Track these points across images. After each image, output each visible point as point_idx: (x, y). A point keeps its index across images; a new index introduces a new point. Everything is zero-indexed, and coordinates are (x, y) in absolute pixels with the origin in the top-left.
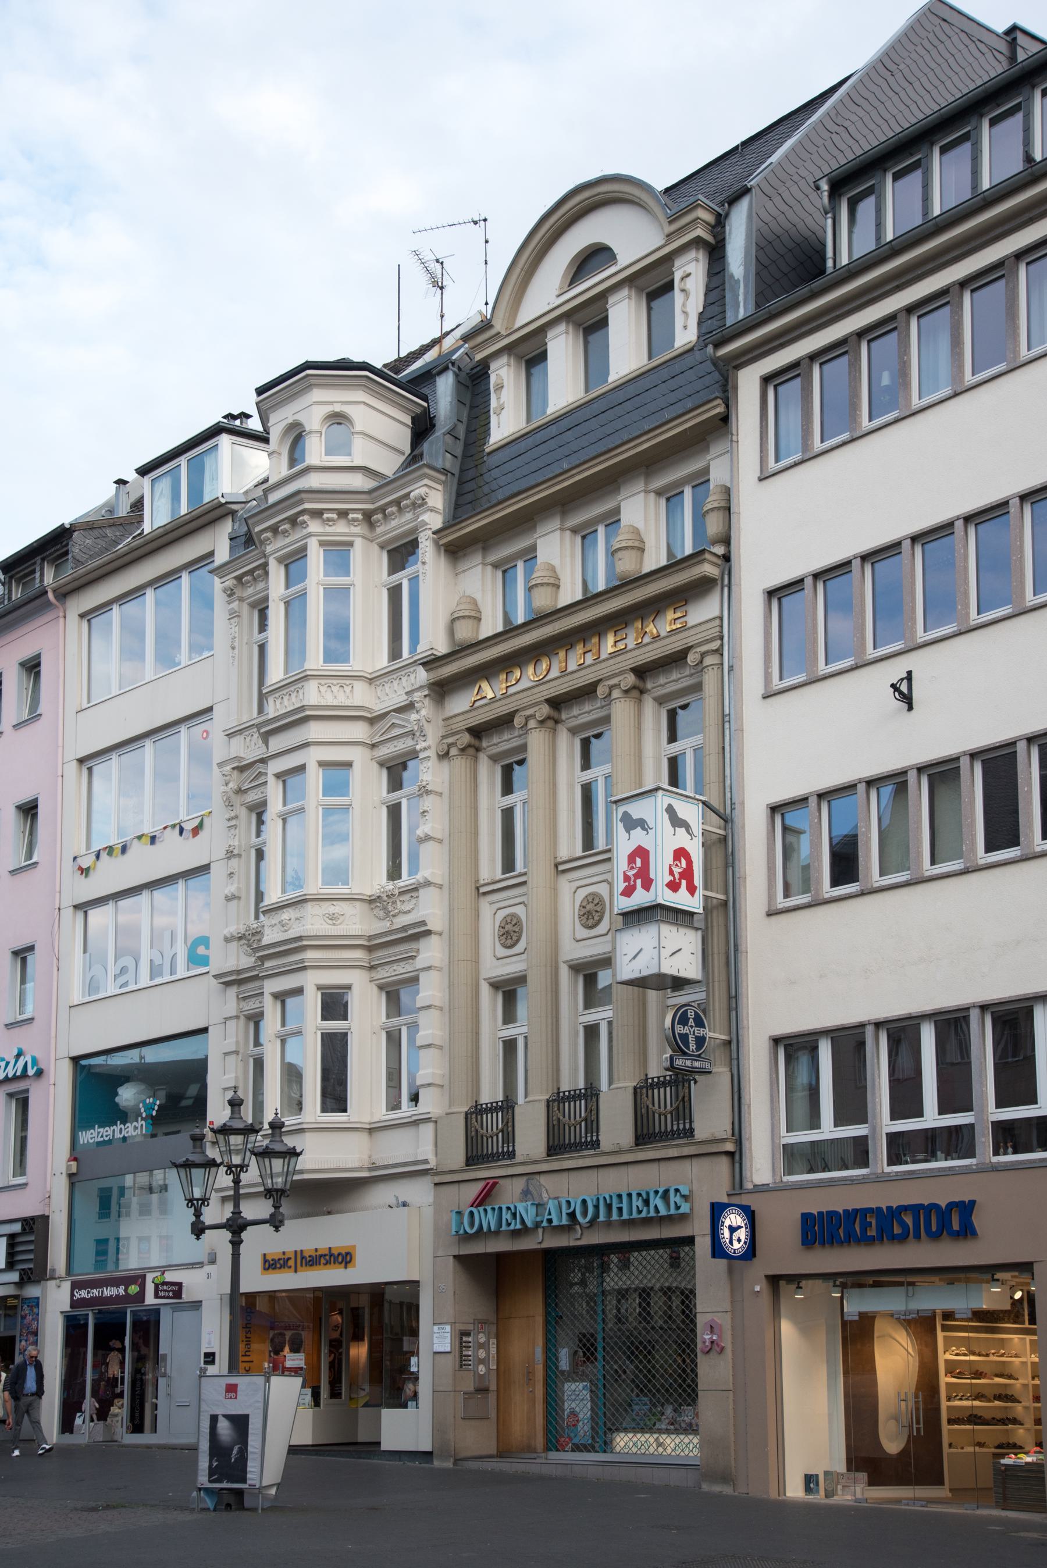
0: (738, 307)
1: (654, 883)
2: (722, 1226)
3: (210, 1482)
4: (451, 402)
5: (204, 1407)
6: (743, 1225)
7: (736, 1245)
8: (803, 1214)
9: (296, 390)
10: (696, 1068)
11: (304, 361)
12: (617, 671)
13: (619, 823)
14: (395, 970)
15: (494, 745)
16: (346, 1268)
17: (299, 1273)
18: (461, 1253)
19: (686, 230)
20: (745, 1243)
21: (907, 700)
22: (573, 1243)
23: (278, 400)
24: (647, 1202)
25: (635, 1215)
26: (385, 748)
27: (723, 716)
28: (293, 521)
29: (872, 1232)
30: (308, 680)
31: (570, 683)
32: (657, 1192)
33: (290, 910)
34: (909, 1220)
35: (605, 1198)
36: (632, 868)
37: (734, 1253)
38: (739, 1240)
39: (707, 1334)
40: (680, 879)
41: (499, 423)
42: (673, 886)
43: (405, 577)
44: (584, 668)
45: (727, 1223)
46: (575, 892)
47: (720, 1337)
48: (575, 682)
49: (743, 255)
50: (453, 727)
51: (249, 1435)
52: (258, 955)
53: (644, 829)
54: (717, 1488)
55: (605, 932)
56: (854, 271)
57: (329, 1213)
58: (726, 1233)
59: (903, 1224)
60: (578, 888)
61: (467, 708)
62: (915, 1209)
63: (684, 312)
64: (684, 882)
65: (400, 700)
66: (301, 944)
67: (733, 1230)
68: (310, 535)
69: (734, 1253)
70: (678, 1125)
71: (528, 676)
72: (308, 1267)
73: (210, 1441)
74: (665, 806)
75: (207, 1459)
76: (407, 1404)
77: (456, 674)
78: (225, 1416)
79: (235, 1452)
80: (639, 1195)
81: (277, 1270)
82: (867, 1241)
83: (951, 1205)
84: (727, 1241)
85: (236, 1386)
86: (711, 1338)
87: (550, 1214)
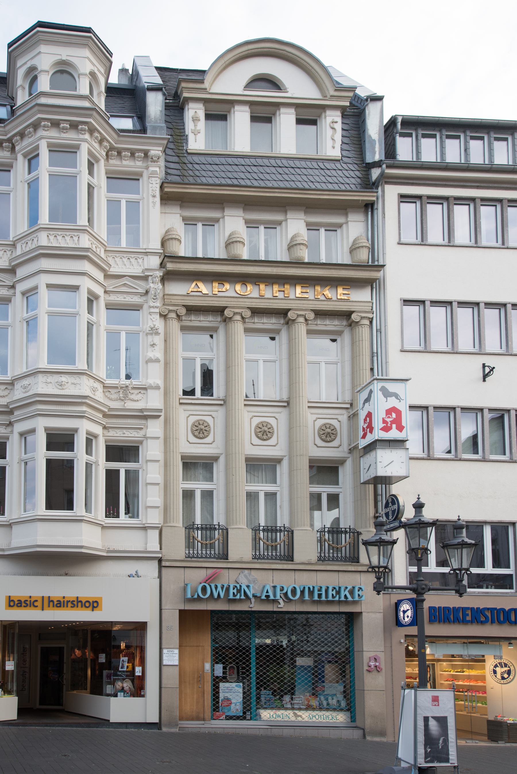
0: (375, 153)
3: (426, 762)
4: (161, 111)
5: (419, 711)
6: (410, 608)
7: (407, 619)
8: (429, 607)
9: (73, 41)
10: (392, 527)
11: (88, 26)
12: (304, 308)
13: (379, 392)
14: (124, 434)
15: (199, 321)
16: (93, 610)
17: (44, 611)
18: (186, 608)
19: (196, 91)
20: (411, 617)
21: (485, 377)
22: (276, 609)
23: (56, 39)
24: (338, 592)
25: (330, 598)
26: (115, 297)
27: (373, 353)
28: (74, 126)
29: (469, 618)
30: (84, 233)
31: (268, 304)
32: (346, 588)
33: (67, 376)
34: (489, 614)
35: (309, 588)
36: (389, 417)
37: (406, 623)
38: (408, 617)
39: (372, 662)
40: (391, 424)
41: (196, 140)
43: (125, 199)
44: (262, 298)
45: (402, 609)
46: (188, 417)
47: (380, 664)
48: (271, 304)
49: (378, 129)
50: (172, 301)
51: (449, 730)
53: (397, 398)
54: (377, 739)
55: (337, 446)
56: (448, 167)
57: (66, 574)
58: (401, 614)
59: (486, 617)
60: (274, 417)
61: (185, 293)
62: (492, 610)
63: (333, 139)
64: (394, 426)
65: (137, 271)
66: (84, 401)
67: (404, 612)
68: (41, 138)
69: (406, 623)
70: (337, 554)
71: (251, 290)
72: (55, 608)
73: (425, 735)
75: (423, 747)
76: (117, 694)
77: (192, 271)
78: (433, 717)
79: (441, 742)
81: (23, 608)
82: (464, 622)
83: (511, 610)
84: (402, 618)
85: (438, 697)
86: (375, 664)
87: (267, 592)
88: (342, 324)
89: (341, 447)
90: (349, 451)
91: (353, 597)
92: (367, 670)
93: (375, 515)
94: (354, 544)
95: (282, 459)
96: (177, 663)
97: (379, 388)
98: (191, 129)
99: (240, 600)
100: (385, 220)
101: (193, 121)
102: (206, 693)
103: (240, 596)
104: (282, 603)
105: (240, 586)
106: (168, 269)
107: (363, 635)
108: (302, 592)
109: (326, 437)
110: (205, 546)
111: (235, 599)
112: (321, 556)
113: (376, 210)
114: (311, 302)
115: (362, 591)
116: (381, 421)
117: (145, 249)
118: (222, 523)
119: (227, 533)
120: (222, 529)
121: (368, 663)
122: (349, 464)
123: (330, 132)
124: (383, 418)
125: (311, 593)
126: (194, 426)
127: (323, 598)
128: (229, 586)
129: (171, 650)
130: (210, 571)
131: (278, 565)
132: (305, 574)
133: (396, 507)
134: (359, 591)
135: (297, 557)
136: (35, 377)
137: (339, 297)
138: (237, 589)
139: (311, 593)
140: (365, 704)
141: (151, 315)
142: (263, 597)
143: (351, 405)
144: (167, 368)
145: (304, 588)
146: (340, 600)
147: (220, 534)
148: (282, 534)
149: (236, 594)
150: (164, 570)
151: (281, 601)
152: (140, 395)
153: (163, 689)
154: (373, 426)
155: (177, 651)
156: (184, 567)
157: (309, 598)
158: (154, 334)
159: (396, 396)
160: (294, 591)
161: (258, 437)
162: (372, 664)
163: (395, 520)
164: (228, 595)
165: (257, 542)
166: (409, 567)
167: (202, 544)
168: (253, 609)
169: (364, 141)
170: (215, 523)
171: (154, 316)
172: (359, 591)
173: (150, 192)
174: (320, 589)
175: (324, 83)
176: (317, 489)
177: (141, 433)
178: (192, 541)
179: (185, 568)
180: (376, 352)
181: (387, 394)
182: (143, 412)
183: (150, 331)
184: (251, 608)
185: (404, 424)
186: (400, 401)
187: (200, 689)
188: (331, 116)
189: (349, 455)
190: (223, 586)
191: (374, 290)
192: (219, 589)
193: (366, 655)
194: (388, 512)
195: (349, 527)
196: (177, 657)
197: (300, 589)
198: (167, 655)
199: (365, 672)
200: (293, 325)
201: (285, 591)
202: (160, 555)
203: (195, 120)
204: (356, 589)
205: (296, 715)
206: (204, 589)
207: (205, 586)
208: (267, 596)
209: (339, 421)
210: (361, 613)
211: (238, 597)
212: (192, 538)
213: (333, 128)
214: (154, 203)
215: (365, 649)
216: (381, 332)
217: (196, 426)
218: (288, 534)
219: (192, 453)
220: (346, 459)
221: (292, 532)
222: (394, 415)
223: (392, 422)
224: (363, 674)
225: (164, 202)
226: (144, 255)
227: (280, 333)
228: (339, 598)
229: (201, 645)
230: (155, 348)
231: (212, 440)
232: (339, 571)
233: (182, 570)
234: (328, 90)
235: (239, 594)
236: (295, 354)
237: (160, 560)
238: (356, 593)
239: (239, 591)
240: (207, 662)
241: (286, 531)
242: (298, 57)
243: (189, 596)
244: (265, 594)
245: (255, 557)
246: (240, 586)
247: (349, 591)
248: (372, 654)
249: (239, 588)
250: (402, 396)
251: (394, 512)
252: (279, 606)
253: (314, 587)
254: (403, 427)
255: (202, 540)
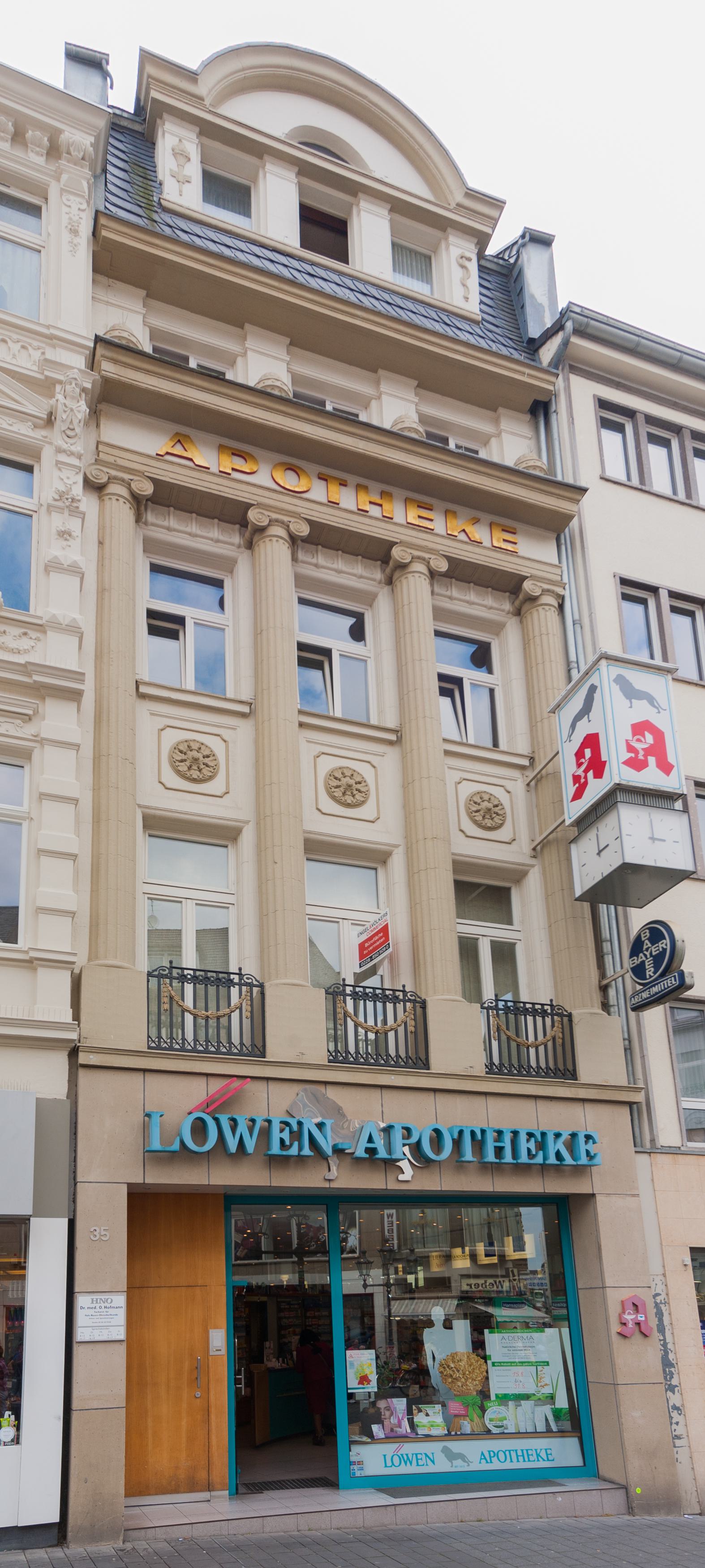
1: (607, 764)
2: (383, 494)
10: (657, 993)
13: (613, 685)
22: (392, 1186)
24: (541, 1146)
25: (524, 1158)
27: (568, 663)
35: (473, 1133)
36: (639, 740)
39: (629, 1314)
40: (645, 756)
42: (636, 764)
47: (646, 1317)
52: (109, 369)
60: (369, 762)
64: (652, 760)
74: (674, 772)
80: (530, 1135)
87: (370, 1140)
88: (503, 607)
89: (514, 843)
90: (533, 853)
91: (574, 1159)
92: (619, 1333)
93: (599, 984)
94: (563, 1039)
95: (388, 854)
96: (120, 1333)
97: (613, 677)
98: (171, 170)
99: (301, 1159)
100: (574, 428)
101: (175, 157)
102: (213, 1410)
103: (300, 1148)
104: (408, 1173)
105: (300, 1124)
106: (103, 372)
107: (603, 1248)
108: (457, 1143)
109: (484, 817)
110: (203, 1022)
111: (287, 1158)
112: (492, 1063)
113: (555, 414)
114: (439, 540)
115: (594, 1142)
116: (623, 747)
117: (48, 327)
118: (251, 969)
119: (263, 994)
120: (251, 985)
121: (620, 1316)
122: (534, 881)
123: (458, 273)
124: (627, 741)
125: (479, 1145)
126: (177, 751)
127: (508, 1158)
128: (269, 1122)
129: (103, 1297)
130: (216, 1085)
131: (393, 1077)
132: (459, 1100)
133: (665, 944)
134: (586, 1143)
135: (437, 1062)
136: (263, 1283)
137: (495, 544)
138: (291, 1132)
139: (479, 1145)
140: (623, 1420)
141: (60, 469)
142: (360, 1153)
143: (532, 759)
144: (103, 599)
145: (461, 1132)
146: (547, 1162)
147: (243, 997)
148: (400, 1007)
149: (287, 1143)
150: (82, 1074)
151: (404, 1165)
152: (25, 639)
153: (75, 1416)
154: (604, 758)
155: (120, 1300)
156: (145, 1071)
157: (473, 1156)
158: (66, 512)
159: (651, 700)
160: (437, 1137)
161: (334, 798)
162: (629, 1317)
163: (663, 975)
164: (268, 1146)
165: (339, 1022)
166: (683, 1099)
167: (195, 1017)
168: (334, 1185)
169: (523, 307)
170: (233, 968)
171: (65, 473)
172: (586, 1143)
173: (65, 221)
174: (500, 1133)
175: (445, 180)
176: (471, 928)
177: (28, 730)
178: (167, 1006)
179: (147, 1075)
180: (575, 660)
181: (631, 693)
182: (30, 676)
183: (56, 500)
184: (330, 1180)
185: (671, 759)
186: (659, 712)
187: (198, 1400)
188: (458, 247)
189: (533, 861)
190: (253, 1121)
191: (563, 548)
192: (242, 1128)
193: (614, 1298)
194: (643, 963)
195: (549, 1003)
196: (120, 1317)
197: (452, 1136)
198: (92, 1312)
199: (615, 1338)
200: (403, 579)
201: (414, 1140)
202: (74, 1036)
203: (180, 155)
204: (581, 1139)
205: (451, 1456)
206: (199, 1129)
207: (201, 1119)
208: (372, 1151)
209: (509, 792)
210: (593, 1195)
211: (294, 1151)
212: (166, 1000)
213: (463, 267)
214: (74, 246)
215: (609, 1282)
216: (581, 628)
217: (181, 752)
218: (414, 1008)
219: (171, 811)
220: (527, 868)
221: (424, 1005)
222: (649, 738)
223: (648, 752)
224: (610, 1344)
225: (102, 279)
226: (47, 344)
227: (375, 604)
228: (545, 1158)
229: (200, 1282)
230: (69, 543)
231: (224, 790)
232: (536, 1097)
233: (138, 1077)
234: (451, 192)
235: (296, 1144)
236: (411, 632)
237: (74, 1053)
238: (582, 1146)
239: (297, 1135)
240: (216, 1327)
241: (409, 1000)
242: (393, 119)
243: (156, 1145)
244: (363, 1144)
245: (335, 1057)
246: (300, 1124)
247: (565, 1144)
248: (626, 1294)
249: (295, 1127)
250: (663, 703)
251: (658, 959)
252: (401, 1177)
253: (483, 1132)
254: (672, 767)
255: (195, 1007)
